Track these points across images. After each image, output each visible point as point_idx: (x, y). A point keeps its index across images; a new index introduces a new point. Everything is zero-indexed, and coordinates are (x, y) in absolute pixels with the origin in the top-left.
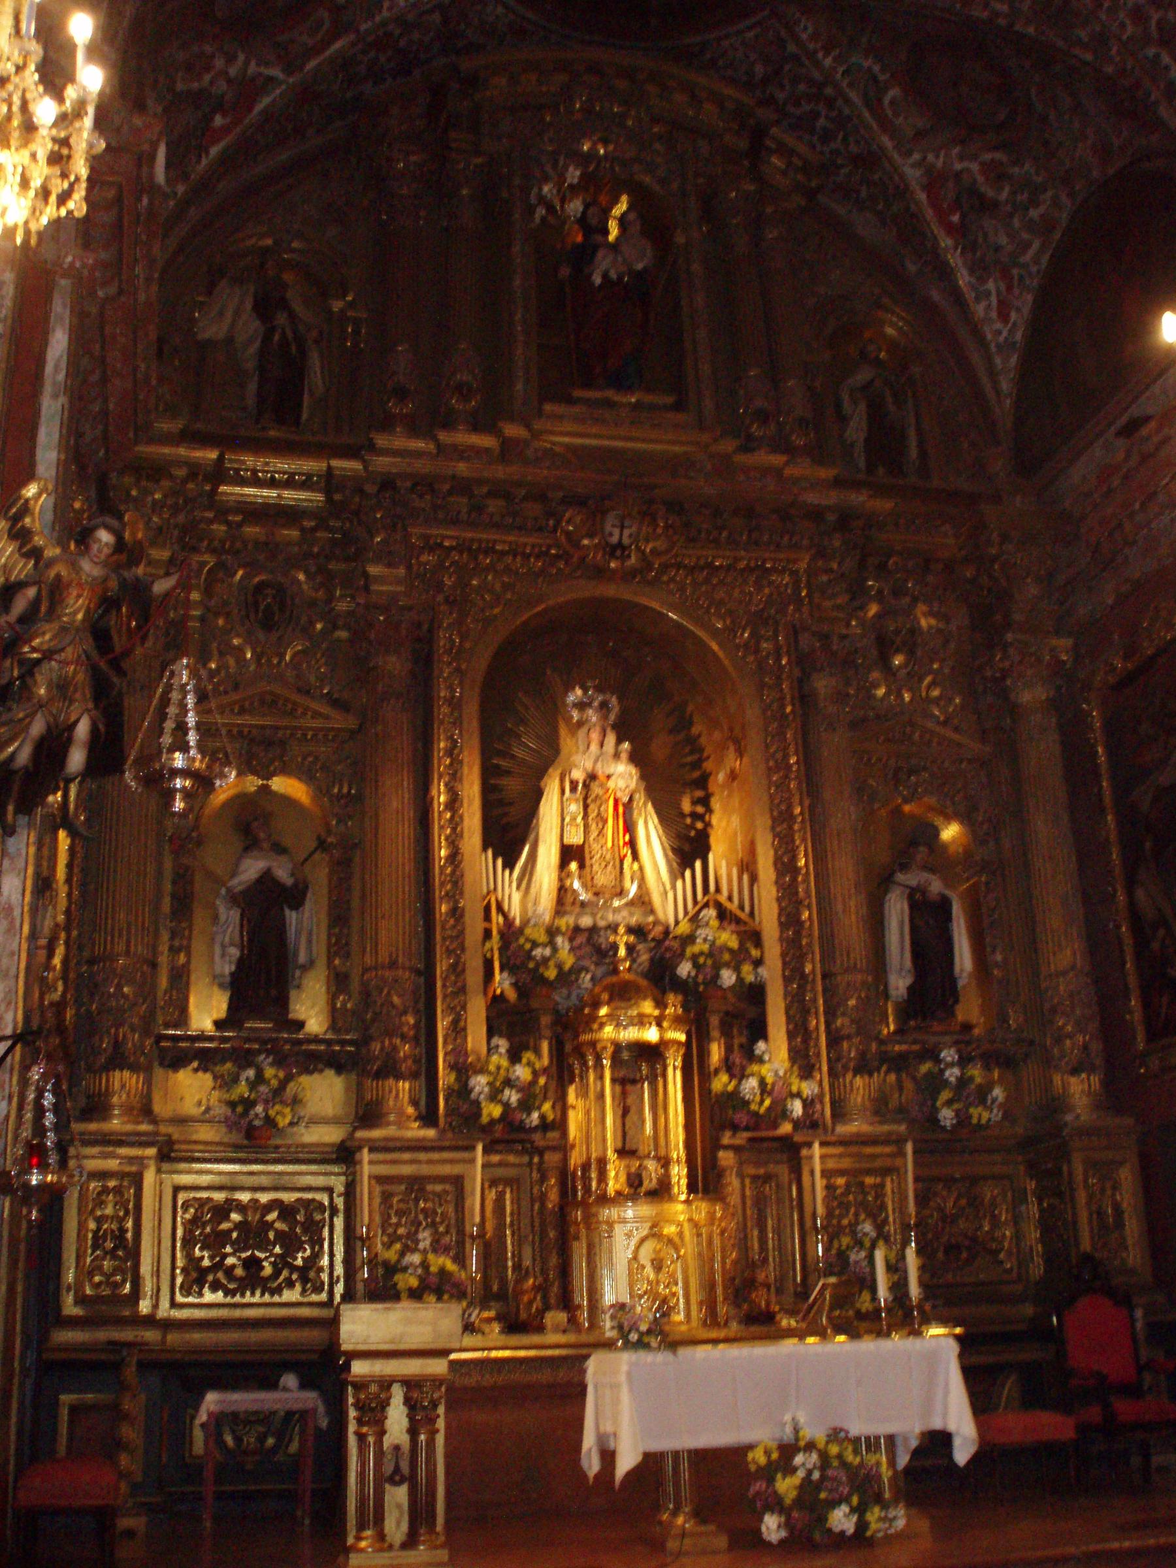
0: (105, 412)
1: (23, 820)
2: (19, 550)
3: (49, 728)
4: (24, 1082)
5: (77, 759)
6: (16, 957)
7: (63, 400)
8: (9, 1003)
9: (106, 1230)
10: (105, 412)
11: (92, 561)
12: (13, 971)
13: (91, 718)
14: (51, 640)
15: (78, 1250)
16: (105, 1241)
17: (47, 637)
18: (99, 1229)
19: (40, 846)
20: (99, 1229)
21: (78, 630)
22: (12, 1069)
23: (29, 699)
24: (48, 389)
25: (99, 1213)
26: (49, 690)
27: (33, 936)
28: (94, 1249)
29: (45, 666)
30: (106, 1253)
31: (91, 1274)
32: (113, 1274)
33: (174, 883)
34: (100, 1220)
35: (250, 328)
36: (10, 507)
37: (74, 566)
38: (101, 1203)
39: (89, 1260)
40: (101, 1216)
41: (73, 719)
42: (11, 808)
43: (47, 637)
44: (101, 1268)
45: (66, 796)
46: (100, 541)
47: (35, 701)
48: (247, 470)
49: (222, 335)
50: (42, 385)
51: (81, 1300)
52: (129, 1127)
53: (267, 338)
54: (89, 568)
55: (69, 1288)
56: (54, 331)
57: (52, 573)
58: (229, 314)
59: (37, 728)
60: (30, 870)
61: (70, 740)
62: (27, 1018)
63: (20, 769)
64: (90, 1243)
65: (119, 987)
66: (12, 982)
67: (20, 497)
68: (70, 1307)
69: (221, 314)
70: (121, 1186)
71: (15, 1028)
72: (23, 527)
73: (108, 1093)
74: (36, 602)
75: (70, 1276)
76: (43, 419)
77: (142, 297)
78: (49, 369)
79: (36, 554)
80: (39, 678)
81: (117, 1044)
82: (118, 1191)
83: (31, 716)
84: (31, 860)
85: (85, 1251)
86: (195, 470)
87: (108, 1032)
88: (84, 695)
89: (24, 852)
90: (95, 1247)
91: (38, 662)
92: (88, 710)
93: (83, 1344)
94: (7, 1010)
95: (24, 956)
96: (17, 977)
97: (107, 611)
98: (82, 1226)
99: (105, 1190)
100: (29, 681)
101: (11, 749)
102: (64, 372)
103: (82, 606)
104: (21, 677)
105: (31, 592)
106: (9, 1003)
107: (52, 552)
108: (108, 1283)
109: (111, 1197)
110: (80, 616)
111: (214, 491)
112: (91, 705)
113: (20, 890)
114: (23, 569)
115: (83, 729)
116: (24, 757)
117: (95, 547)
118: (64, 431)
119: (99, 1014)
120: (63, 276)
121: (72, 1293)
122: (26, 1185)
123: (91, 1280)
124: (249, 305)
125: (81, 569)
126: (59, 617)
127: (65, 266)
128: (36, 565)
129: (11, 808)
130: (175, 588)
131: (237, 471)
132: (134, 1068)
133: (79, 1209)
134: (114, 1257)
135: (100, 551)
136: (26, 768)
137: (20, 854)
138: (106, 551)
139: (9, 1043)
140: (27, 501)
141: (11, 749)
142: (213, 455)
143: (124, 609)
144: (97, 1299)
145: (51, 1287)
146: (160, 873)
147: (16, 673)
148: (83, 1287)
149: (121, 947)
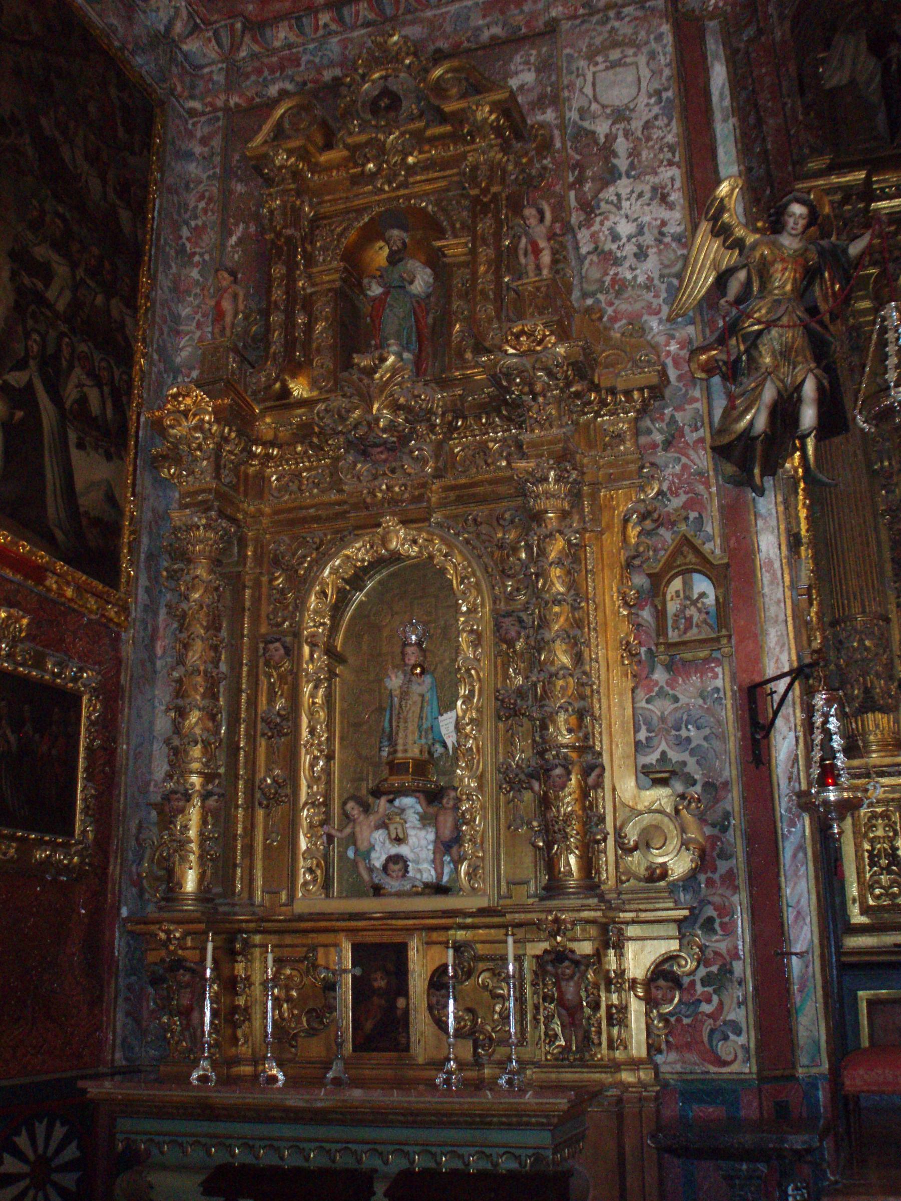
0: (765, 152)
1: (769, 482)
2: (724, 242)
3: (779, 392)
4: (809, 710)
5: (808, 416)
6: (782, 605)
7: (732, 121)
8: (783, 645)
9: (879, 850)
10: (765, 152)
11: (791, 235)
12: (782, 617)
13: (816, 377)
14: (767, 313)
15: (857, 868)
16: (880, 858)
17: (763, 311)
18: (873, 849)
19: (786, 502)
20: (873, 849)
21: (789, 300)
22: (794, 703)
23: (757, 369)
24: (718, 115)
25: (871, 835)
26: (774, 356)
27: (793, 586)
28: (871, 867)
29: (765, 339)
30: (882, 869)
31: (871, 887)
32: (891, 887)
33: (892, 549)
34: (872, 841)
35: (869, 65)
36: (709, 209)
37: (774, 245)
38: (872, 827)
39: (868, 875)
40: (875, 837)
41: (799, 380)
42: (757, 471)
43: (763, 311)
44: (878, 882)
45: (804, 457)
46: (794, 214)
47: (763, 370)
48: (890, 187)
49: (844, 82)
50: (713, 114)
51: (866, 910)
52: (888, 760)
53: (886, 70)
54: (789, 242)
55: (854, 901)
56: (713, 65)
57: (757, 255)
58: (848, 60)
59: (769, 394)
60: (782, 527)
61: (800, 400)
62: (799, 658)
63: (760, 436)
64: (867, 861)
65: (861, 641)
66: (782, 627)
67: (715, 199)
68: (857, 917)
69: (842, 61)
70: (887, 810)
71: (791, 664)
72: (723, 223)
73: (864, 734)
74: (749, 282)
75: (853, 890)
76: (719, 140)
77: (778, 35)
78: (715, 99)
79: (739, 244)
80: (763, 349)
81: (867, 691)
82: (885, 815)
83: (761, 385)
84: (782, 517)
85: (864, 868)
86: (847, 193)
87: (857, 681)
88: (805, 357)
89: (774, 511)
90: (872, 864)
91: (760, 333)
92: (811, 370)
93: (873, 947)
94: (781, 651)
95: (789, 602)
96: (786, 621)
97: (810, 283)
98: (858, 847)
99: (874, 816)
100: (755, 354)
101: (748, 417)
102: (728, 99)
103: (789, 278)
104: (747, 351)
105: (742, 275)
106: (783, 646)
107: (751, 239)
108: (887, 895)
109: (880, 821)
110: (788, 287)
111: (867, 209)
112: (813, 365)
113: (776, 545)
114: (730, 258)
115: (809, 389)
116: (761, 424)
117: (791, 221)
118: (739, 146)
119: (847, 666)
120: (710, 19)
121: (857, 905)
122: (826, 802)
123: (872, 894)
124: (863, 46)
125: (782, 245)
126: (771, 292)
127: (711, 9)
128: (740, 254)
129: (757, 471)
130: (871, 240)
131: (882, 190)
132: (884, 710)
133: (854, 833)
134: (890, 872)
135: (796, 223)
136: (765, 432)
137: (770, 514)
138: (802, 222)
139: (787, 680)
140: (722, 200)
141: (748, 417)
142: (862, 175)
143: (826, 274)
144: (880, 909)
145: (838, 899)
146: (879, 544)
147: (742, 348)
148: (866, 899)
149: (856, 609)
